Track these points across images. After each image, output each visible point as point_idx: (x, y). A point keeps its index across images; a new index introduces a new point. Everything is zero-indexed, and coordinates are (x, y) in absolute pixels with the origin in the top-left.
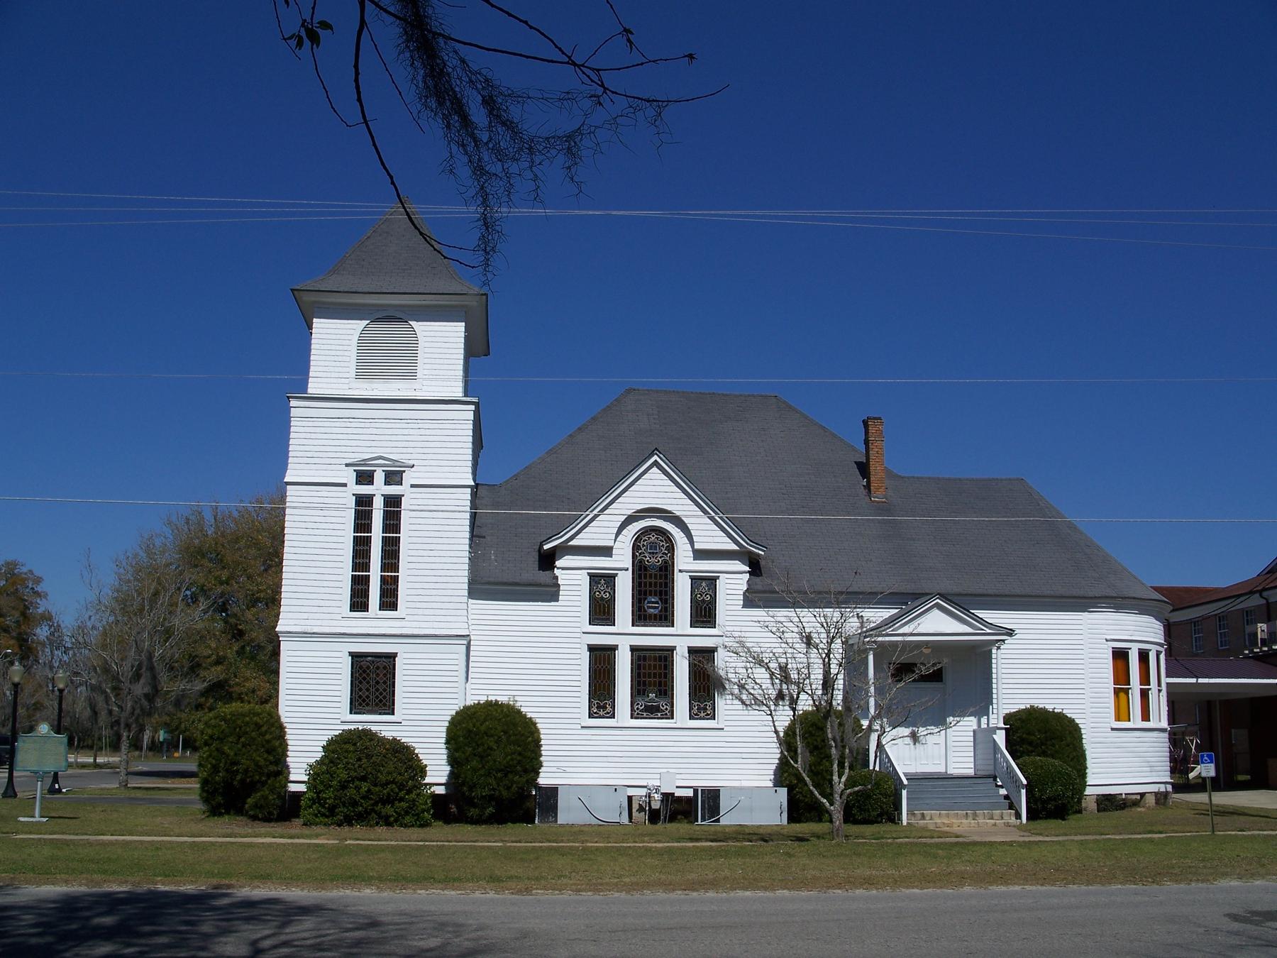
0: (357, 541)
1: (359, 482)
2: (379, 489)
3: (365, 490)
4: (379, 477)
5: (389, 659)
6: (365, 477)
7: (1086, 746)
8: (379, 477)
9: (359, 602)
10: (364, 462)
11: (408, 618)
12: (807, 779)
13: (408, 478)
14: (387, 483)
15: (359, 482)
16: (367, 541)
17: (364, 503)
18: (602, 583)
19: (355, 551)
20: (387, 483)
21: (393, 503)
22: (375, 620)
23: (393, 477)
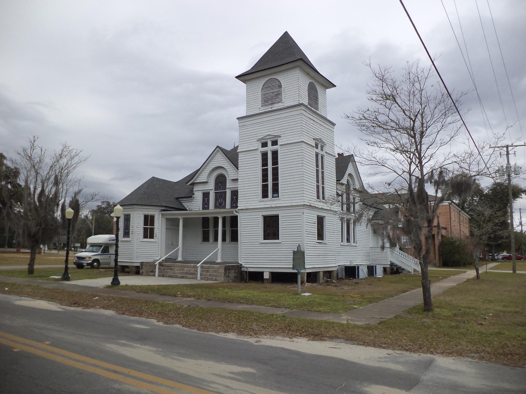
0: (263, 170)
1: (262, 147)
2: (270, 148)
3: (265, 149)
4: (269, 144)
5: (276, 217)
6: (264, 145)
7: (275, 346)
8: (269, 144)
9: (265, 195)
10: (262, 139)
11: (258, 202)
12: (72, 309)
13: (279, 143)
14: (272, 145)
15: (262, 147)
16: (267, 170)
17: (264, 156)
18: (206, 195)
19: (263, 174)
20: (272, 145)
21: (275, 154)
22: (270, 202)
23: (275, 143)
